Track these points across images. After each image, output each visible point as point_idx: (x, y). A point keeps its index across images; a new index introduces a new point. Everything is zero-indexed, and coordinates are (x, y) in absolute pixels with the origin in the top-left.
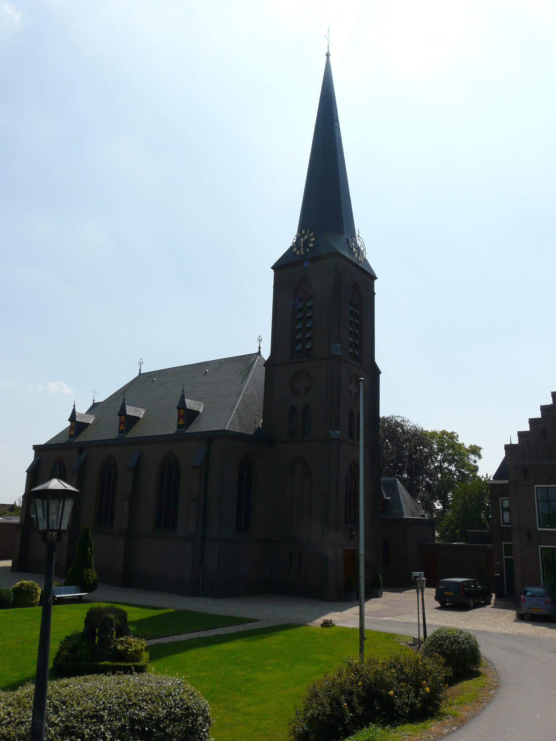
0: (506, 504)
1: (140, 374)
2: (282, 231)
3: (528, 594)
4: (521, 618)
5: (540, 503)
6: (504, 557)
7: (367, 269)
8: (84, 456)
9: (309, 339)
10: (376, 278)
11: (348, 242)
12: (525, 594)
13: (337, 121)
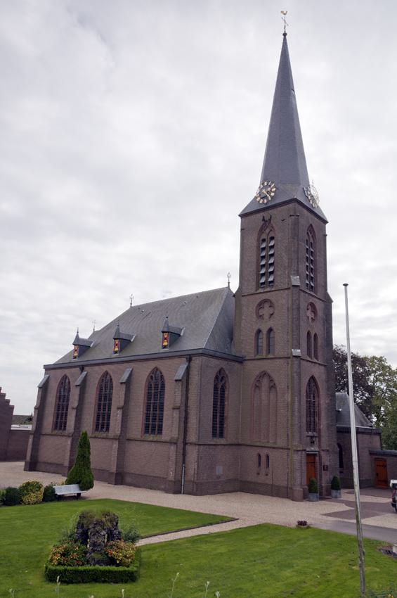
1: (131, 307)
2: (247, 185)
7: (322, 216)
8: (85, 373)
9: (272, 273)
10: (327, 222)
11: (304, 191)
13: (293, 84)
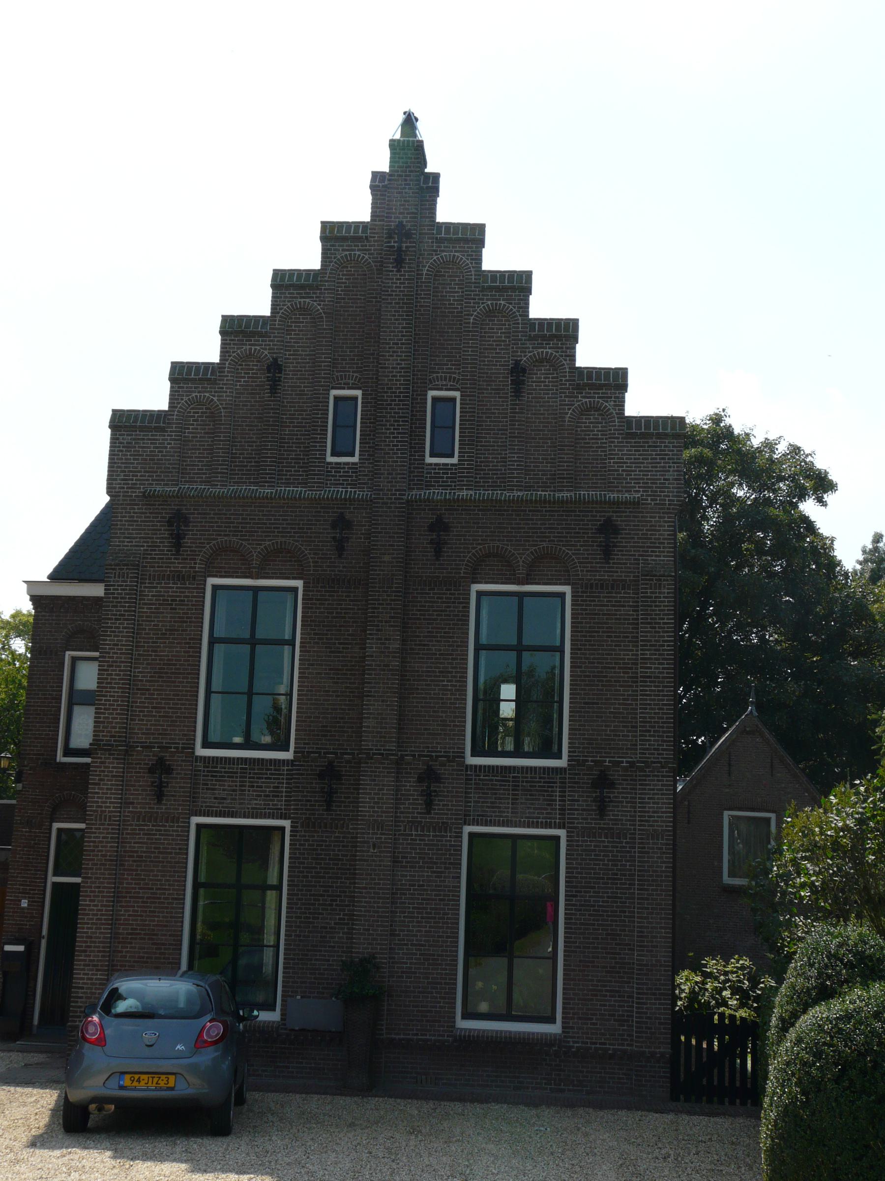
0: (88, 677)
3: (122, 1007)
4: (76, 1123)
5: (216, 699)
6: (52, 879)
12: (107, 1008)
